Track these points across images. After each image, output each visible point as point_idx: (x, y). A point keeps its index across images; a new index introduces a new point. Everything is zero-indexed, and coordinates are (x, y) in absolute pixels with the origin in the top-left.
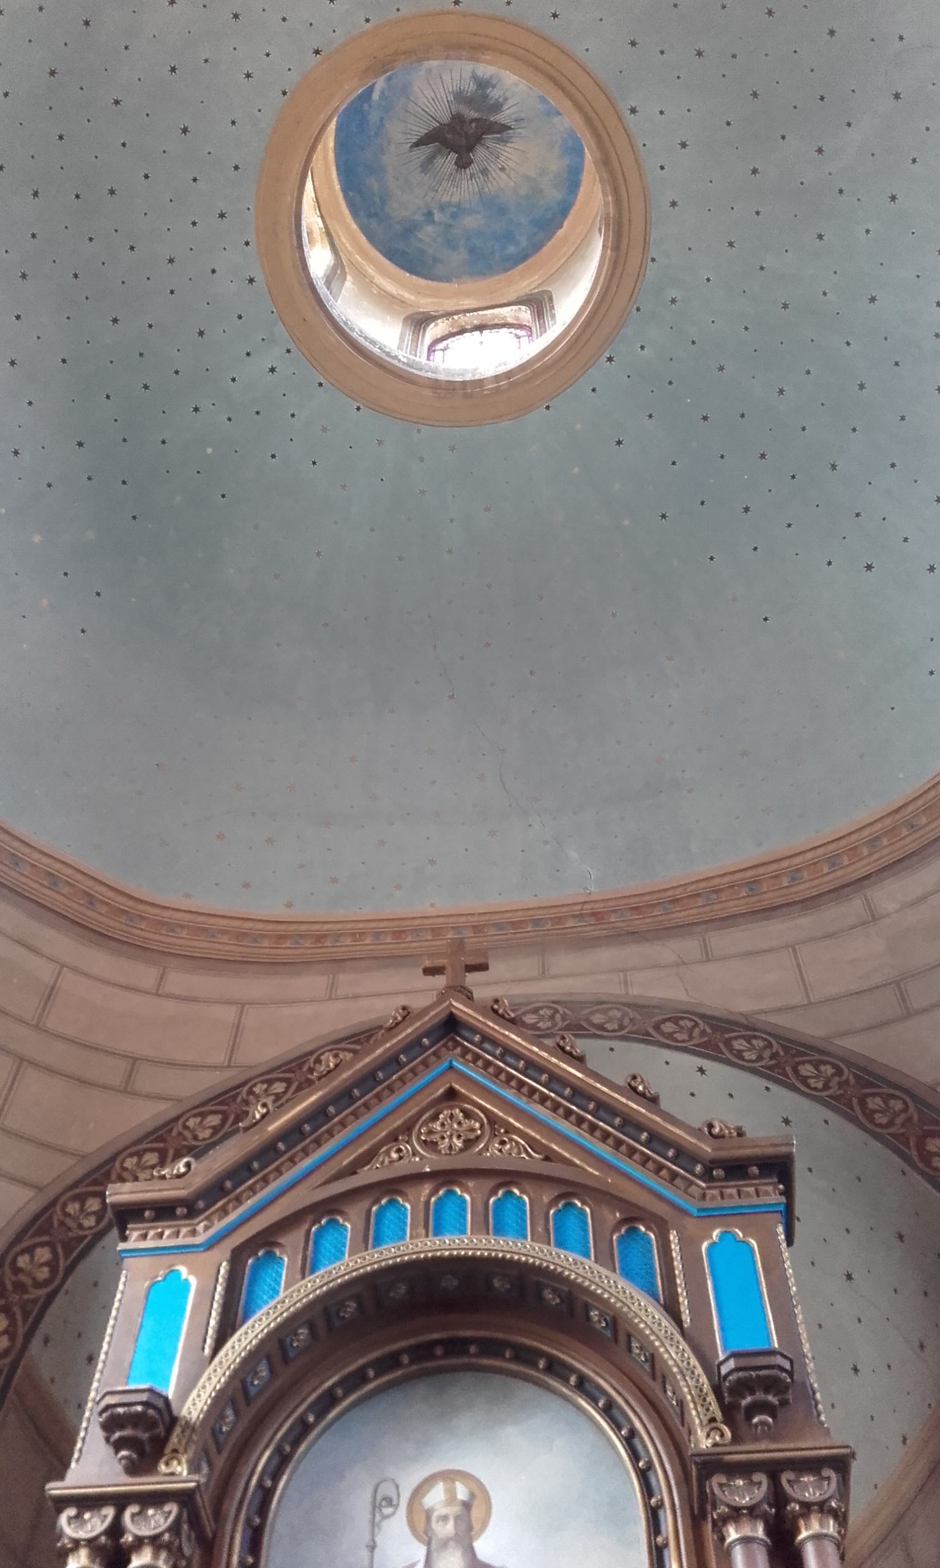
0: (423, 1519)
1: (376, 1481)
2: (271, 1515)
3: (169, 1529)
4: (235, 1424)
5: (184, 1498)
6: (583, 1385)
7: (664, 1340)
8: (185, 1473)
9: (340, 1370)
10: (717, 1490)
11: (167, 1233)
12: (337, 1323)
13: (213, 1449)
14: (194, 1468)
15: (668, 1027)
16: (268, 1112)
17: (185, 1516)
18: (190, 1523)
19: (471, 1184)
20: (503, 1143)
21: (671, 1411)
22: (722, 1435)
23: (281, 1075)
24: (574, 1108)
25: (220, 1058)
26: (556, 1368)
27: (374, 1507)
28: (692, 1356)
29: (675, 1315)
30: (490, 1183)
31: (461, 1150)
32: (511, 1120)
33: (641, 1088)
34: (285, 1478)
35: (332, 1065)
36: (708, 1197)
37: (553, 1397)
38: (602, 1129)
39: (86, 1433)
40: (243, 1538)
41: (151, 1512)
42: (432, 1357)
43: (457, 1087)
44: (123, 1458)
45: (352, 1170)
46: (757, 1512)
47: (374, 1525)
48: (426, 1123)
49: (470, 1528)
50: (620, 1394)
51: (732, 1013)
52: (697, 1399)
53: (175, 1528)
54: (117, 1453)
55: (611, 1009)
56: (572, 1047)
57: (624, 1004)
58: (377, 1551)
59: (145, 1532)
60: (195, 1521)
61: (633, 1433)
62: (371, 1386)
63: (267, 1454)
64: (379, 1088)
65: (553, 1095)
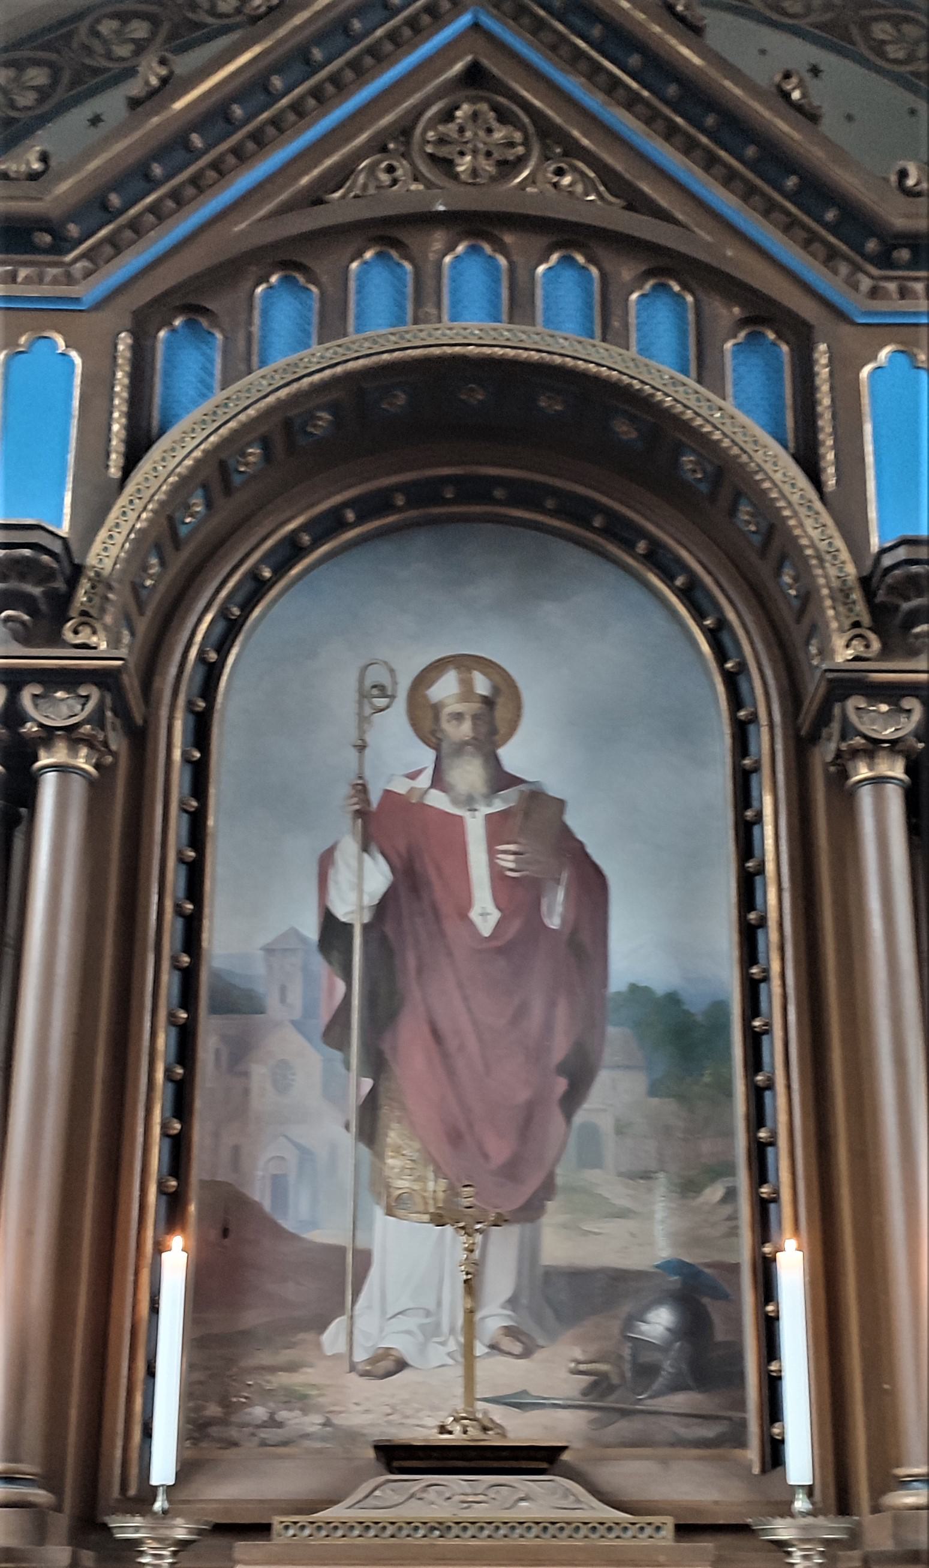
1: (363, 662)
2: (220, 699)
4: (158, 578)
5: (106, 679)
8: (103, 646)
10: (853, 717)
11: (23, 273)
12: (302, 441)
13: (133, 609)
14: (115, 642)
18: (114, 711)
19: (508, 239)
20: (560, 172)
24: (679, 120)
26: (621, 532)
29: (814, 475)
30: (542, 241)
31: (493, 179)
32: (576, 133)
33: (796, 95)
34: (234, 651)
35: (154, 81)
36: (48, 279)
37: (609, 567)
38: (726, 165)
40: (185, 724)
41: (59, 694)
42: (439, 500)
43: (486, 62)
45: (314, 198)
47: (363, 721)
48: (432, 124)
49: (493, 731)
50: (710, 573)
53: (97, 719)
58: (367, 751)
60: (122, 711)
61: (722, 623)
63: (209, 618)
65: (646, 93)
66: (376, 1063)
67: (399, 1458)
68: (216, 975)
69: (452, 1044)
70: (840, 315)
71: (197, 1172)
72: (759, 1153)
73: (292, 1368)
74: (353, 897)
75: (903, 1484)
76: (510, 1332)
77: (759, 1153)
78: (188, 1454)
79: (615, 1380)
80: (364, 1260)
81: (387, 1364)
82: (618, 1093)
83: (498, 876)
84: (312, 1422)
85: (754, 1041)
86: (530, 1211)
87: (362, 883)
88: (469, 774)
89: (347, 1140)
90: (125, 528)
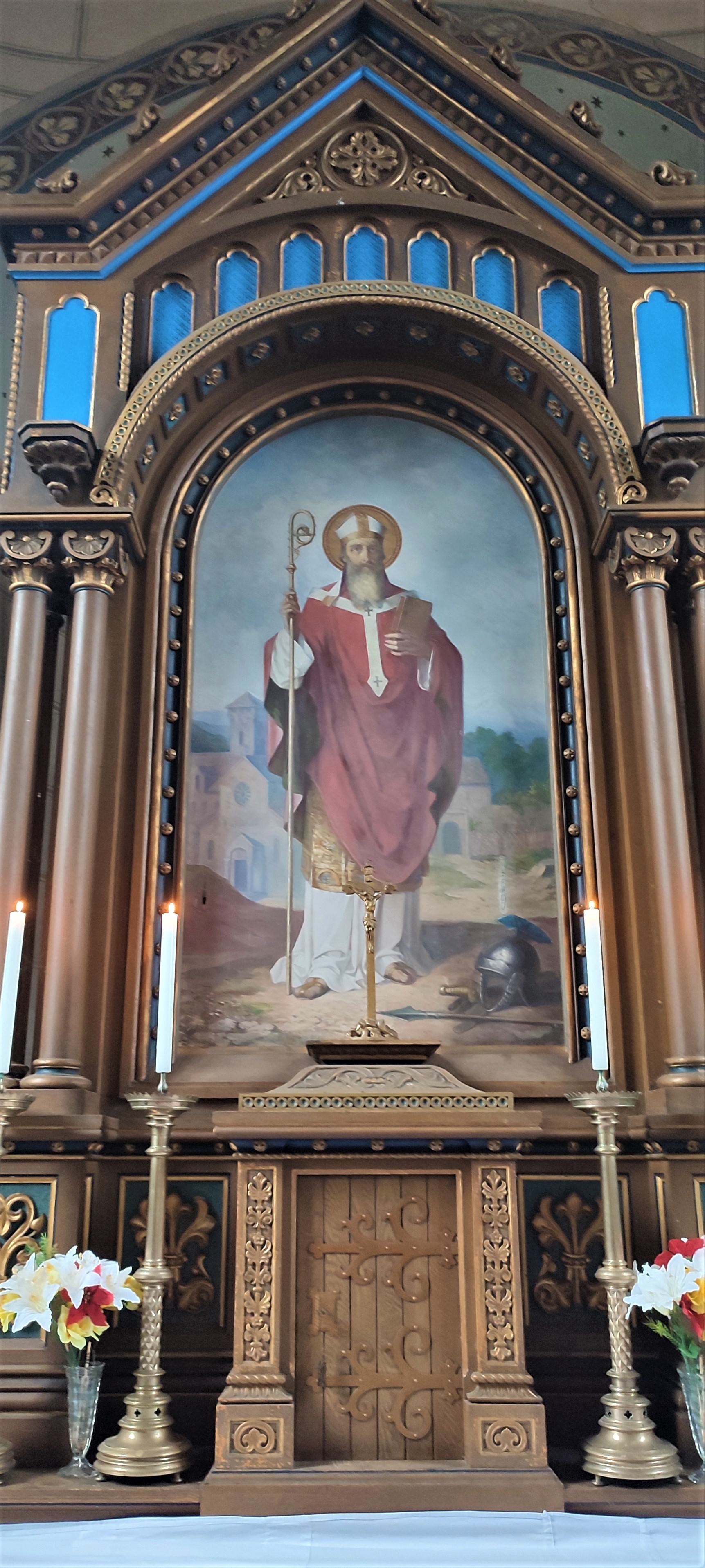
0: (339, 546)
1: (293, 512)
3: (106, 555)
5: (118, 527)
6: (494, 437)
7: (588, 399)
8: (117, 505)
9: (255, 408)
11: (60, 255)
12: (249, 363)
14: (125, 501)
15: (568, 47)
16: (158, 119)
17: (121, 542)
19: (388, 222)
20: (422, 176)
21: (580, 467)
22: (638, 493)
23: (138, 75)
25: (65, 47)
27: (293, 535)
28: (616, 417)
32: (433, 150)
33: (584, 119)
34: (206, 506)
39: (10, 460)
42: (343, 400)
43: (371, 104)
44: (53, 487)
45: (256, 199)
46: (662, 562)
49: (382, 557)
51: (639, 33)
52: (617, 459)
53: (113, 554)
54: (46, 483)
55: (506, 19)
56: (507, 62)
57: (521, 14)
59: (86, 556)
60: (130, 548)
61: (538, 479)
62: (284, 425)
64: (282, 98)
65: (480, 121)
66: (305, 784)
67: (326, 1053)
68: (195, 726)
69: (356, 770)
70: (617, 267)
71: (184, 860)
72: (569, 843)
73: (250, 992)
74: (288, 671)
75: (672, 1069)
76: (398, 966)
77: (569, 843)
78: (180, 1051)
79: (472, 999)
80: (298, 919)
81: (316, 989)
82: (470, 802)
83: (386, 656)
84: (264, 1029)
85: (564, 766)
86: (412, 883)
87: (293, 662)
88: (365, 586)
89: (286, 836)
90: (130, 425)
